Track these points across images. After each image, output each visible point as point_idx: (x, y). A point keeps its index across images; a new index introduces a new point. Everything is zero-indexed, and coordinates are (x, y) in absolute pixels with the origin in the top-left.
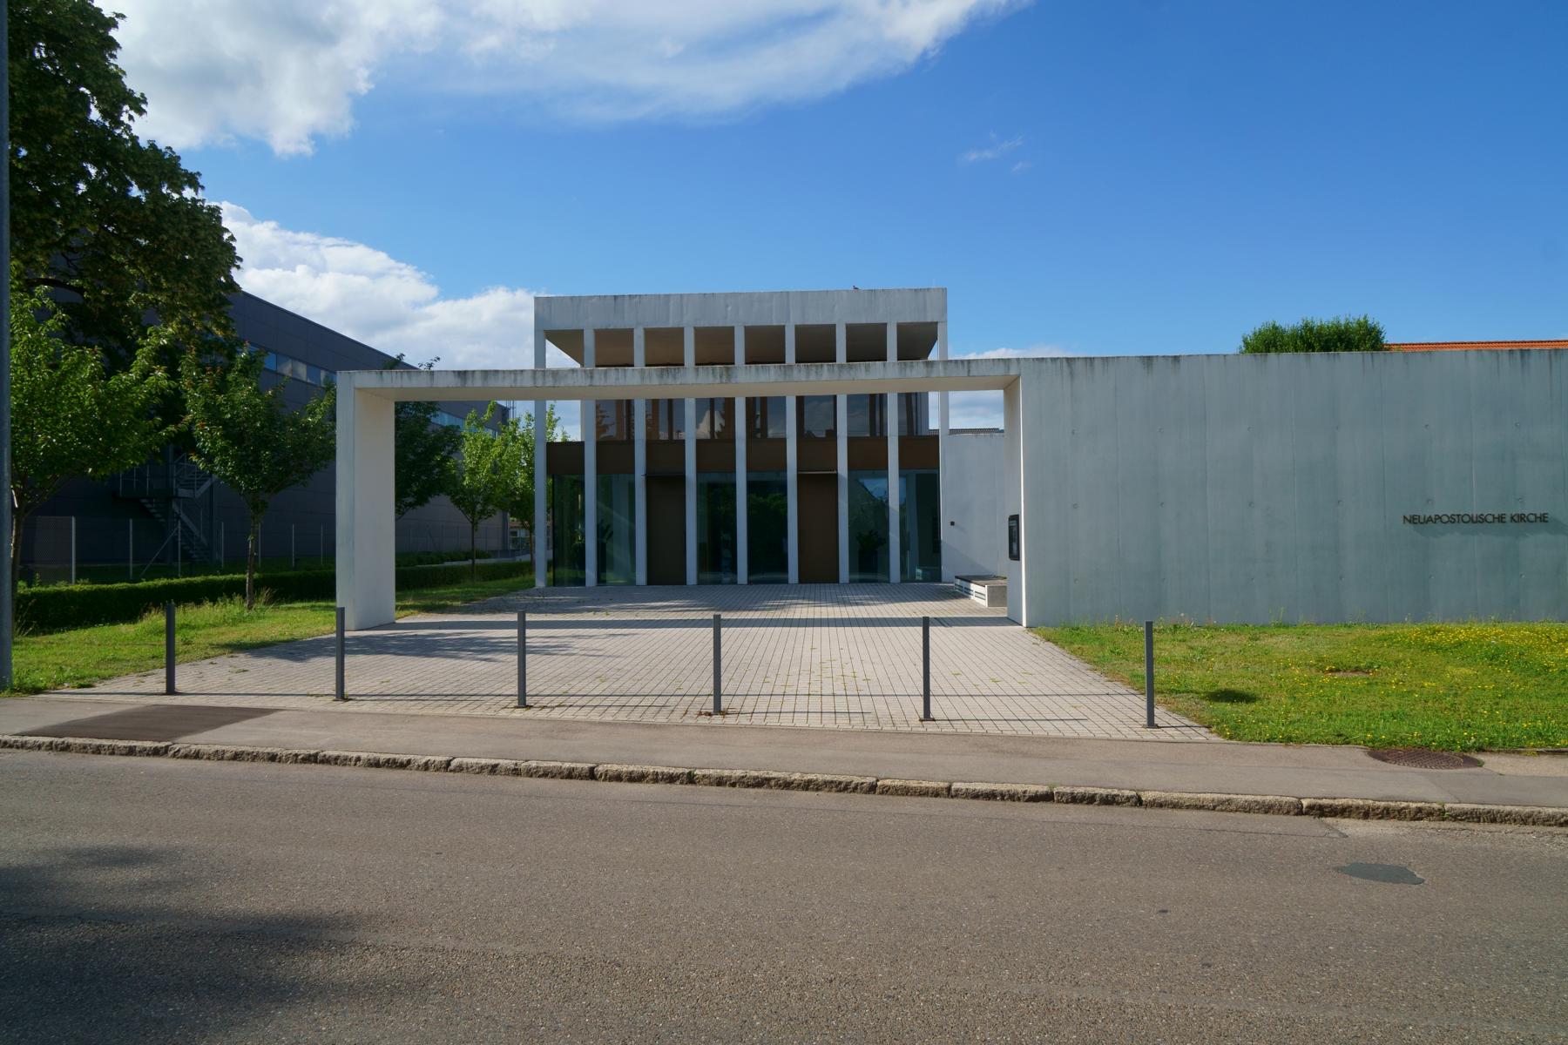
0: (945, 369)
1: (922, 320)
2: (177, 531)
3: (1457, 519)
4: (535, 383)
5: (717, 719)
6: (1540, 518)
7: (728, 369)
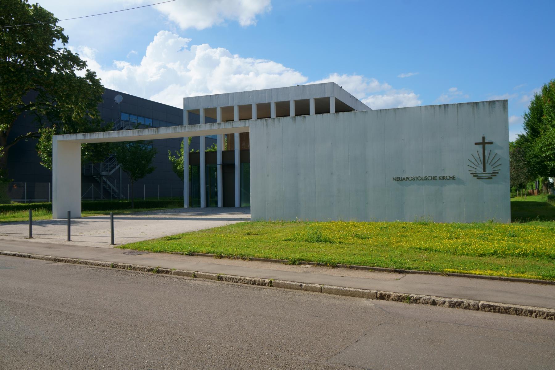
0: (224, 125)
1: (323, 97)
2: (92, 187)
3: (415, 179)
5: (31, 240)
6: (452, 178)
7: (157, 129)
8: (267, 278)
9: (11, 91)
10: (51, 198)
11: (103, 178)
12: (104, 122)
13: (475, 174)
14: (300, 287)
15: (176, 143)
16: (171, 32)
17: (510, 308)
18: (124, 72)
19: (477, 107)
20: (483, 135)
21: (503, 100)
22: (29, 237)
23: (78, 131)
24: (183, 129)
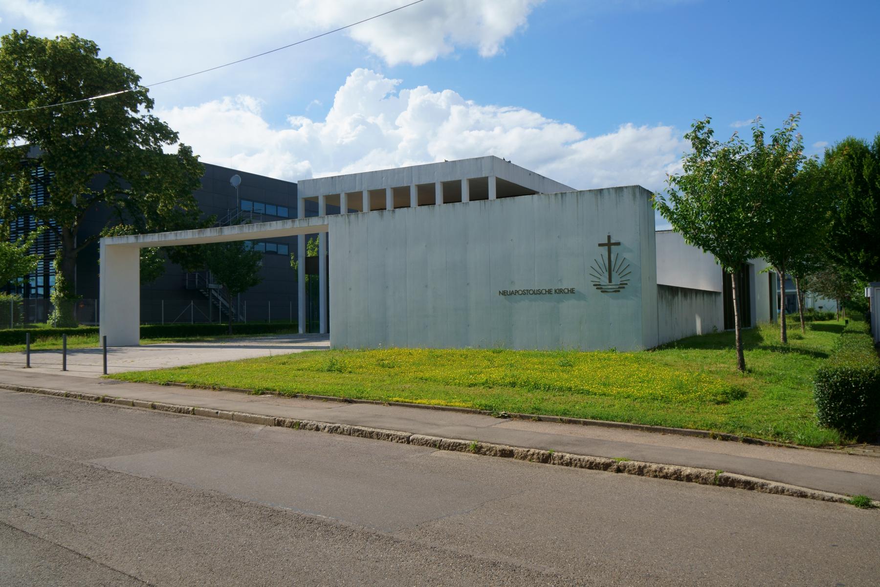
0: (299, 223)
1: (479, 176)
4: (159, 239)
5: (64, 373)
8: (503, 443)
9: (70, 178)
10: (98, 321)
11: (213, 292)
12: (204, 214)
13: (598, 286)
14: (216, 415)
15: (291, 242)
16: (372, 71)
17: (373, 432)
18: (303, 131)
19: (601, 195)
20: (609, 233)
21: (633, 186)
22: (26, 367)
23: (165, 229)
24: (251, 229)
